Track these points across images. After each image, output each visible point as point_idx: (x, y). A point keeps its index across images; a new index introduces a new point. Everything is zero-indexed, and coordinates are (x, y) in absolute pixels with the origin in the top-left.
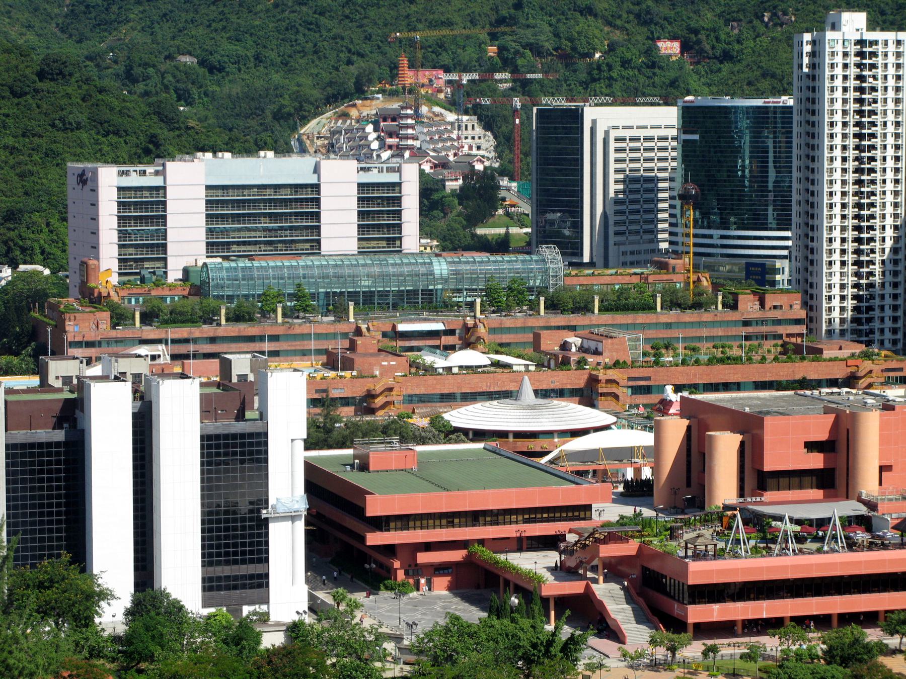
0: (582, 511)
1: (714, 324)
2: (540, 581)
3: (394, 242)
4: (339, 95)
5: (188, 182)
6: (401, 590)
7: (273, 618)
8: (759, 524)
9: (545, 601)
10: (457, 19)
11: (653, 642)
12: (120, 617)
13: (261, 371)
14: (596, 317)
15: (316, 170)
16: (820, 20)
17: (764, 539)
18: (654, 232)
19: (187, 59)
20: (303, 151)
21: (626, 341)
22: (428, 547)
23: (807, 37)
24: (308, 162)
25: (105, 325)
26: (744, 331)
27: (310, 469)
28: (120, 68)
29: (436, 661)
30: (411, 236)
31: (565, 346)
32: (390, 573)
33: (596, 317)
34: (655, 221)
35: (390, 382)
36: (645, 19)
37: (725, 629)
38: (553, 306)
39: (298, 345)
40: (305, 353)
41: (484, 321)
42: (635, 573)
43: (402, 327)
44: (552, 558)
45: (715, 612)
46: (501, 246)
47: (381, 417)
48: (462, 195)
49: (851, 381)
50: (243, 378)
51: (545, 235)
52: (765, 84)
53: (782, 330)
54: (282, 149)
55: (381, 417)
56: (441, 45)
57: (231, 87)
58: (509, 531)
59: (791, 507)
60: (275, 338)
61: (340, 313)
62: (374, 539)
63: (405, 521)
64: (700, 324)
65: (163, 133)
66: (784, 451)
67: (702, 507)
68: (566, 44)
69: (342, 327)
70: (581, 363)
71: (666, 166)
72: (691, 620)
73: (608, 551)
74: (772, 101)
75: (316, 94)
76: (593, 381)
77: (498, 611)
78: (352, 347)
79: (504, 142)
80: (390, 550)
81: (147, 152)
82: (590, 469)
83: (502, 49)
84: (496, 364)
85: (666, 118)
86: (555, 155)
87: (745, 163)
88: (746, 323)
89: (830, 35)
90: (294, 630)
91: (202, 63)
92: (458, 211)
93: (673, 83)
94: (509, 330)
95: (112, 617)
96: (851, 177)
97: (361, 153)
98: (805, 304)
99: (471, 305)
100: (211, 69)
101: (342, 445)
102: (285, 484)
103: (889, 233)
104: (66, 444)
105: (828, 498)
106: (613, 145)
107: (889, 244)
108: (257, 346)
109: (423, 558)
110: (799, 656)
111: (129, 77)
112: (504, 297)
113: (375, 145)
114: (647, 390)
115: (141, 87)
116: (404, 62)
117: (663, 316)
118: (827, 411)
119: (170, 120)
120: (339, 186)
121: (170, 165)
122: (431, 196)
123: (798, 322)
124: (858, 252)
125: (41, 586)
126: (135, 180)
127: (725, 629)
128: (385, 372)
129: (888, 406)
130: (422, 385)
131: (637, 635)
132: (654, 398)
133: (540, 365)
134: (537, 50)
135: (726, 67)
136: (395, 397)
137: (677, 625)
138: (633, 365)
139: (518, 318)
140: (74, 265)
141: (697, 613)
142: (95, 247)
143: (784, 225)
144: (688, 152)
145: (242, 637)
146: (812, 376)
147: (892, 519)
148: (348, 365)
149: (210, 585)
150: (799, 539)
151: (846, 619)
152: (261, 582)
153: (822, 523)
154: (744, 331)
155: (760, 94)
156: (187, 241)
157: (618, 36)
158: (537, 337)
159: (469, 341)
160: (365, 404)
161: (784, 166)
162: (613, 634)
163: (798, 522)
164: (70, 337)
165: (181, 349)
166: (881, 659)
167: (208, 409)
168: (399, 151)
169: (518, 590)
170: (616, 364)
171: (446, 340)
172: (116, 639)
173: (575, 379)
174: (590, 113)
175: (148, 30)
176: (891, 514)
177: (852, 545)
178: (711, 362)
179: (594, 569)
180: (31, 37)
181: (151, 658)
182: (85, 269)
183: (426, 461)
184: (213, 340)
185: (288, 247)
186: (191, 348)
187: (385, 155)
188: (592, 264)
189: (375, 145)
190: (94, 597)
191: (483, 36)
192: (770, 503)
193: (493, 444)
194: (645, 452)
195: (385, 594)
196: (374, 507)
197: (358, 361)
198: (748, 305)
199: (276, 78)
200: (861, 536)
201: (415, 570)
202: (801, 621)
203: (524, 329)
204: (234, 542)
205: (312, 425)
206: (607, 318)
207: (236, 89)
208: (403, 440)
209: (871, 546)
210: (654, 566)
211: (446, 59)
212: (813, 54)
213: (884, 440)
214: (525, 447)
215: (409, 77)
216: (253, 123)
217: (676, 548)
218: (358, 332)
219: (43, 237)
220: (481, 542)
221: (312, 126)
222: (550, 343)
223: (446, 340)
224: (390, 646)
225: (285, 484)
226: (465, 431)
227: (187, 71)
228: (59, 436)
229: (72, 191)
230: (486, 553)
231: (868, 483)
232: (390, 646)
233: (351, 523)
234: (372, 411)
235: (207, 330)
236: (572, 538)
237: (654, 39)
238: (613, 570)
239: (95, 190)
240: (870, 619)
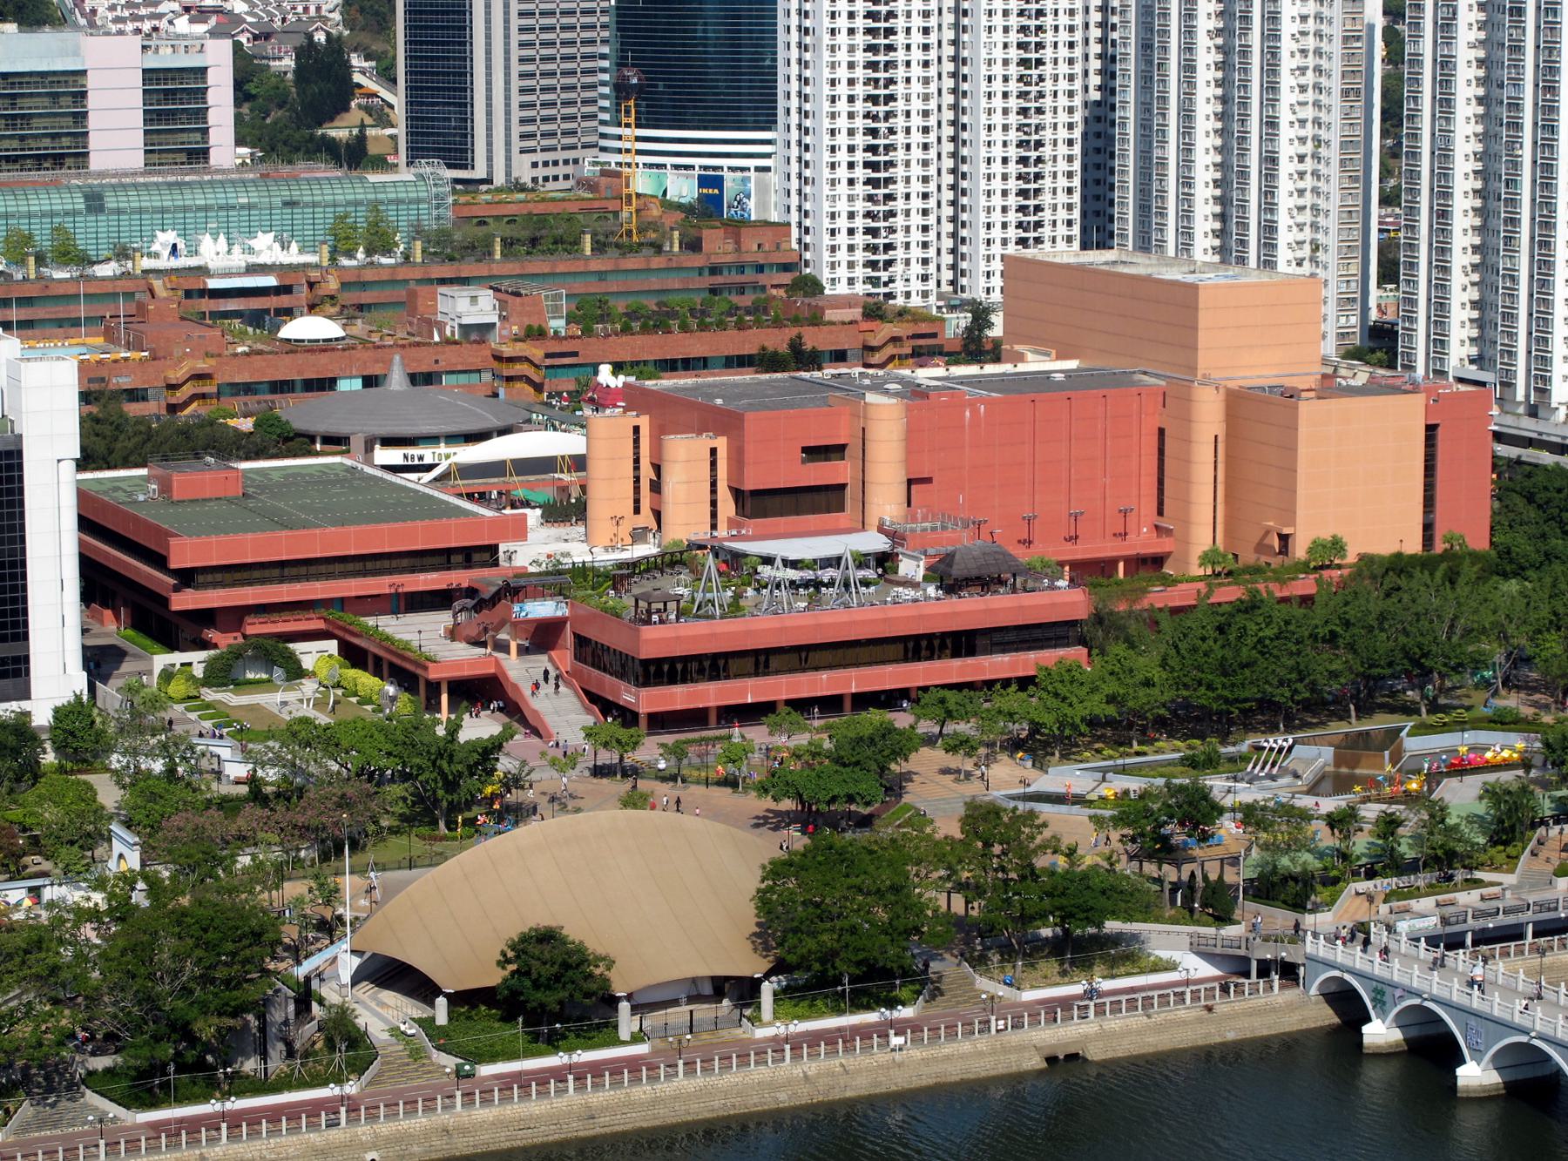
88: (715, 270)
151: (864, 701)
240: (889, 699)
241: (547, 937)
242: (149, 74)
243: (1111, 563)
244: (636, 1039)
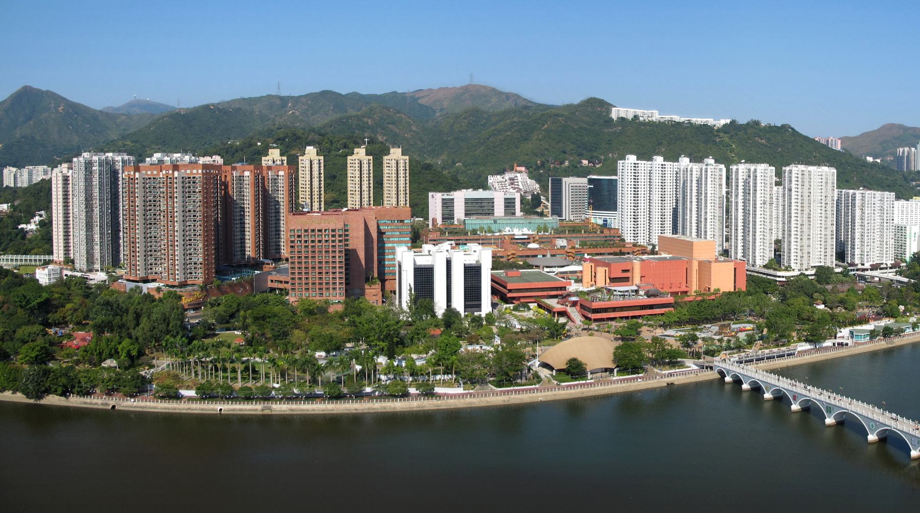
5: (460, 197)
27: (492, 275)
44: (556, 300)
45: (599, 316)
58: (545, 293)
72: (463, 217)
85: (584, 181)
126: (446, 197)
149: (466, 307)
151: (633, 317)
183: (522, 274)
202: (622, 318)
235: (466, 237)
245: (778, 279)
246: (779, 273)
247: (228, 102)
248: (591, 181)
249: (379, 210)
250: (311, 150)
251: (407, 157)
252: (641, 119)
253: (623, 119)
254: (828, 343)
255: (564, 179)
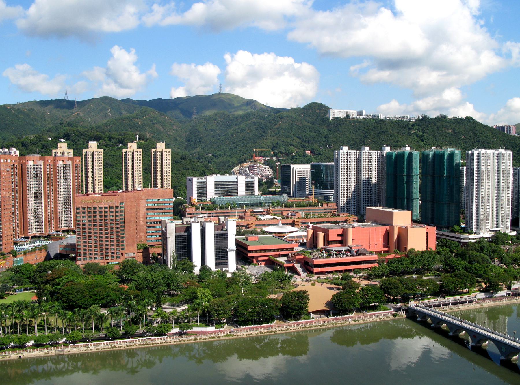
0: (292, 249)
1: (318, 209)
2: (284, 263)
3: (253, 193)
4: (241, 162)
5: (211, 181)
6: (255, 265)
7: (229, 271)
8: (328, 251)
9: (285, 267)
10: (265, 146)
11: (307, 276)
12: (199, 271)
13: (226, 220)
14: (294, 208)
15: (237, 178)
16: (339, 148)
17: (329, 255)
18: (305, 190)
19: (210, 155)
20: (234, 174)
21: (300, 213)
22: (260, 256)
23: (336, 151)
24: (235, 176)
25: (194, 210)
26: (324, 211)
27: (236, 240)
28: (197, 157)
29: (262, 280)
30: (256, 192)
31: (288, 214)
32: (253, 262)
33: (294, 208)
34: (305, 188)
35: (252, 222)
36: (303, 147)
37: (321, 273)
38: (285, 206)
39: (234, 214)
40: (235, 216)
41: (271, 209)
42: (303, 262)
43: (255, 210)
44: (286, 259)
46: (274, 193)
47: (250, 229)
48: (266, 182)
49: (346, 221)
50: (223, 222)
51: (283, 191)
52: (327, 160)
53: (332, 211)
54: (230, 174)
55: (250, 229)
56: (262, 152)
57: (219, 160)
59: (335, 248)
60: (229, 213)
61: (242, 208)
62: (250, 255)
63: (256, 251)
64: (316, 210)
65: (206, 170)
66: (333, 236)
67: (316, 248)
68: (287, 152)
69: (242, 211)
70: (291, 218)
71: (308, 176)
73: (297, 257)
74: (329, 164)
75: (237, 162)
76: (294, 221)
77: (275, 270)
78: (244, 215)
79: (275, 171)
80: (253, 257)
81: (203, 174)
82: (292, 240)
83: (274, 153)
84: (274, 218)
85: (308, 167)
86: (285, 174)
87: (324, 175)
88: (325, 209)
89: (341, 151)
90: (233, 274)
91: (213, 155)
92: (266, 186)
93: (309, 160)
94: (276, 211)
95: (197, 271)
96: (346, 180)
97: (246, 175)
98: (336, 205)
99: (269, 206)
100: (215, 157)
101: (243, 235)
102: (232, 245)
103: (353, 186)
104: (187, 235)
105: (341, 246)
106: (297, 172)
107: (353, 189)
108: (225, 214)
109: (260, 259)
110: (336, 278)
111: (199, 159)
112: (275, 204)
113: (248, 172)
114: (305, 223)
115: (201, 161)
116: (254, 155)
117: (308, 208)
118: (342, 228)
119: (207, 168)
120: (242, 181)
121: (207, 177)
122: (260, 181)
123: (335, 209)
124: (347, 190)
125: (182, 264)
126: (200, 180)
127: (321, 273)
128: (251, 220)
129: (354, 227)
130: (259, 223)
131: (304, 275)
132: (306, 225)
133: (283, 218)
134: (281, 153)
135: (319, 156)
136: (253, 225)
137: (311, 272)
138: (302, 218)
139: (278, 208)
140: (188, 197)
141: (316, 270)
142: (192, 194)
143: (332, 188)
144: (312, 174)
145: (223, 275)
146: (338, 220)
147: (355, 250)
148: (244, 218)
149: (217, 264)
150: (336, 255)
151: (346, 271)
152: (226, 264)
153: (341, 251)
154: (324, 211)
155: (327, 162)
156: (211, 193)
157: (298, 150)
158: (282, 213)
159: (268, 213)
160: (247, 226)
161: (332, 175)
162: (299, 274)
163: (336, 251)
164: (187, 213)
165: (210, 215)
166: (353, 279)
167: (216, 228)
168: (253, 173)
169: (279, 265)
170: (298, 218)
171: (263, 213)
172: (198, 275)
173: (290, 221)
174: (293, 166)
175: (202, 149)
176: (355, 249)
177: (347, 256)
178: (317, 217)
179: (295, 261)
180: (179, 150)
181: (205, 279)
182: (190, 199)
183: (260, 238)
184: (216, 213)
185: (231, 194)
186: (212, 215)
187: (251, 174)
188: (293, 197)
189: (248, 172)
190: (193, 267)
191: (270, 150)
192: (330, 247)
193: (274, 235)
194: (305, 236)
195: (251, 266)
196: (249, 249)
197: (246, 218)
198: (325, 206)
199: (228, 158)
200: (349, 254)
201: (258, 261)
203: (279, 211)
204: (221, 255)
205: (237, 231)
206: (296, 208)
207: (220, 161)
208: (255, 234)
209: (351, 256)
210: (307, 260)
211: (263, 155)
212: (337, 155)
213: (353, 234)
214: (280, 235)
215: (255, 158)
216: (224, 168)
217: (311, 257)
218: (246, 211)
219: (182, 192)
220: (271, 255)
221: (236, 168)
222: (285, 214)
223: (263, 213)
224: (253, 277)
225: (232, 245)
226: (268, 232)
227: (210, 157)
228: (186, 234)
229: (188, 183)
230: (272, 258)
231: (350, 243)
232: (253, 277)
233: (245, 251)
234: (249, 228)
236: (290, 255)
237: (305, 151)
238: (298, 261)
239: (192, 182)
240: (349, 271)
241: (307, 298)
242: (246, 181)
243: (381, 251)
244: (313, 318)
245: (462, 241)
246: (462, 236)
247: (23, 104)
248: (313, 167)
249: (148, 192)
250: (93, 145)
251: (170, 150)
252: (351, 117)
253: (337, 118)
254: (503, 293)
255: (293, 166)
